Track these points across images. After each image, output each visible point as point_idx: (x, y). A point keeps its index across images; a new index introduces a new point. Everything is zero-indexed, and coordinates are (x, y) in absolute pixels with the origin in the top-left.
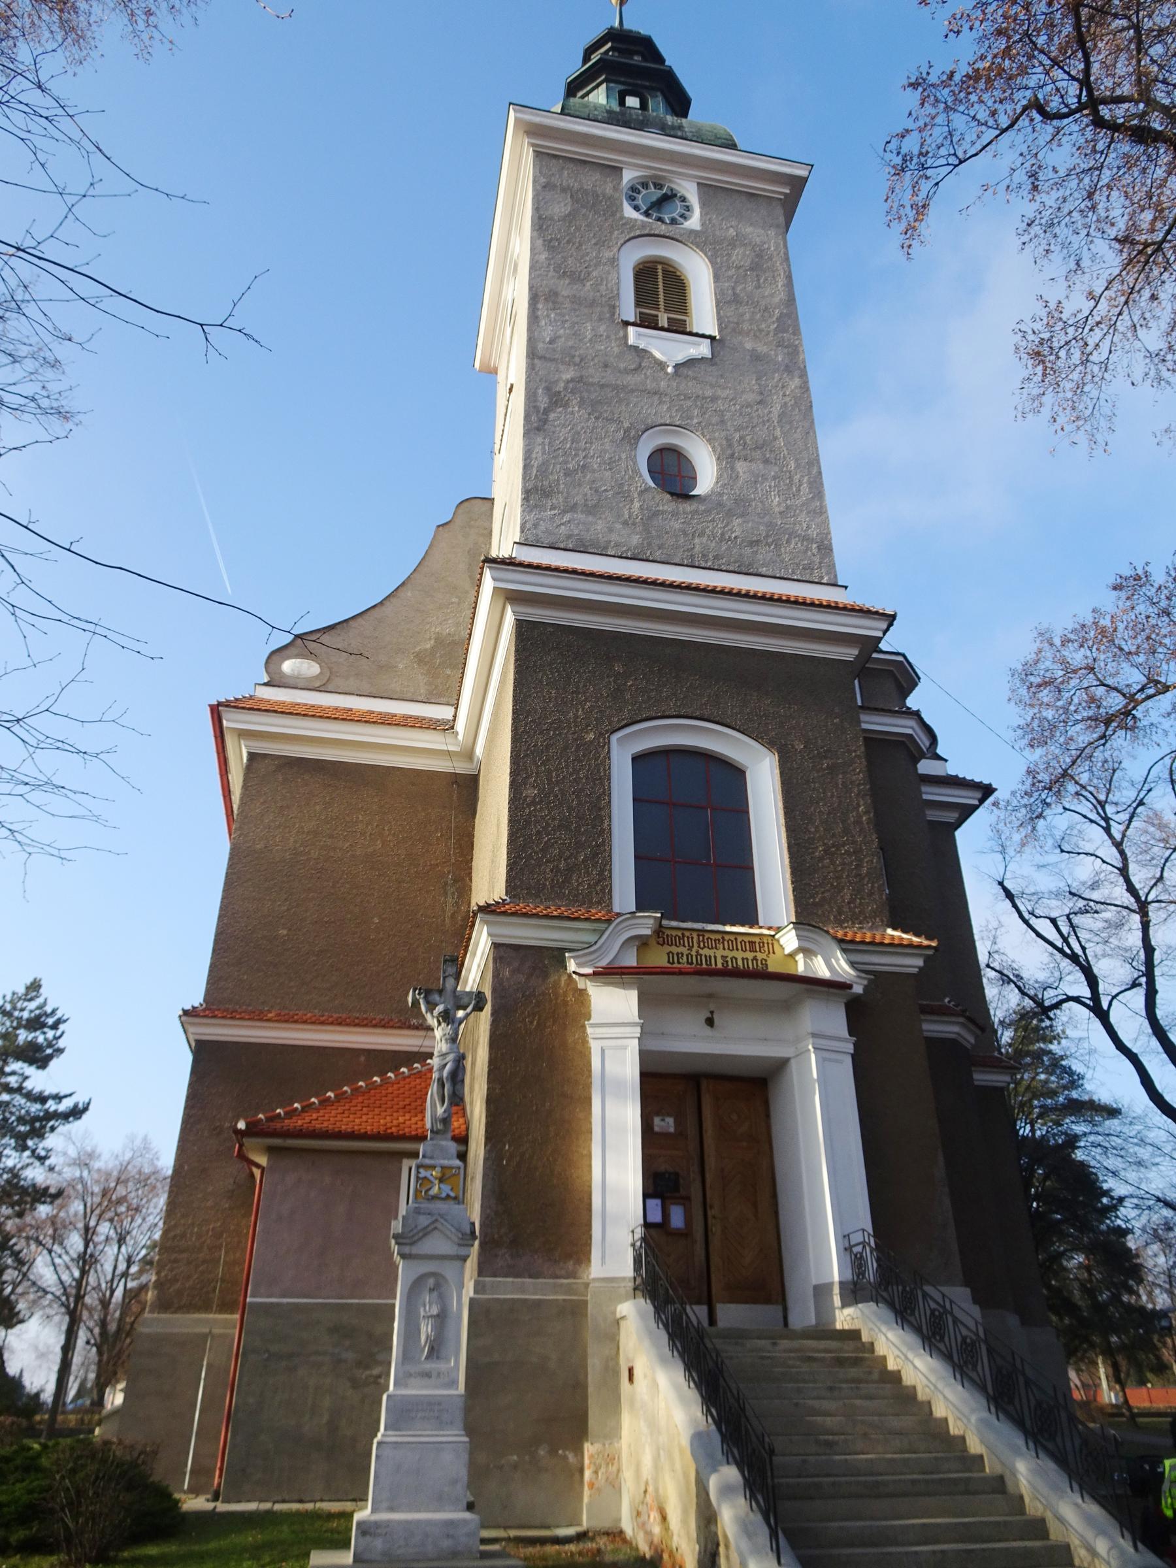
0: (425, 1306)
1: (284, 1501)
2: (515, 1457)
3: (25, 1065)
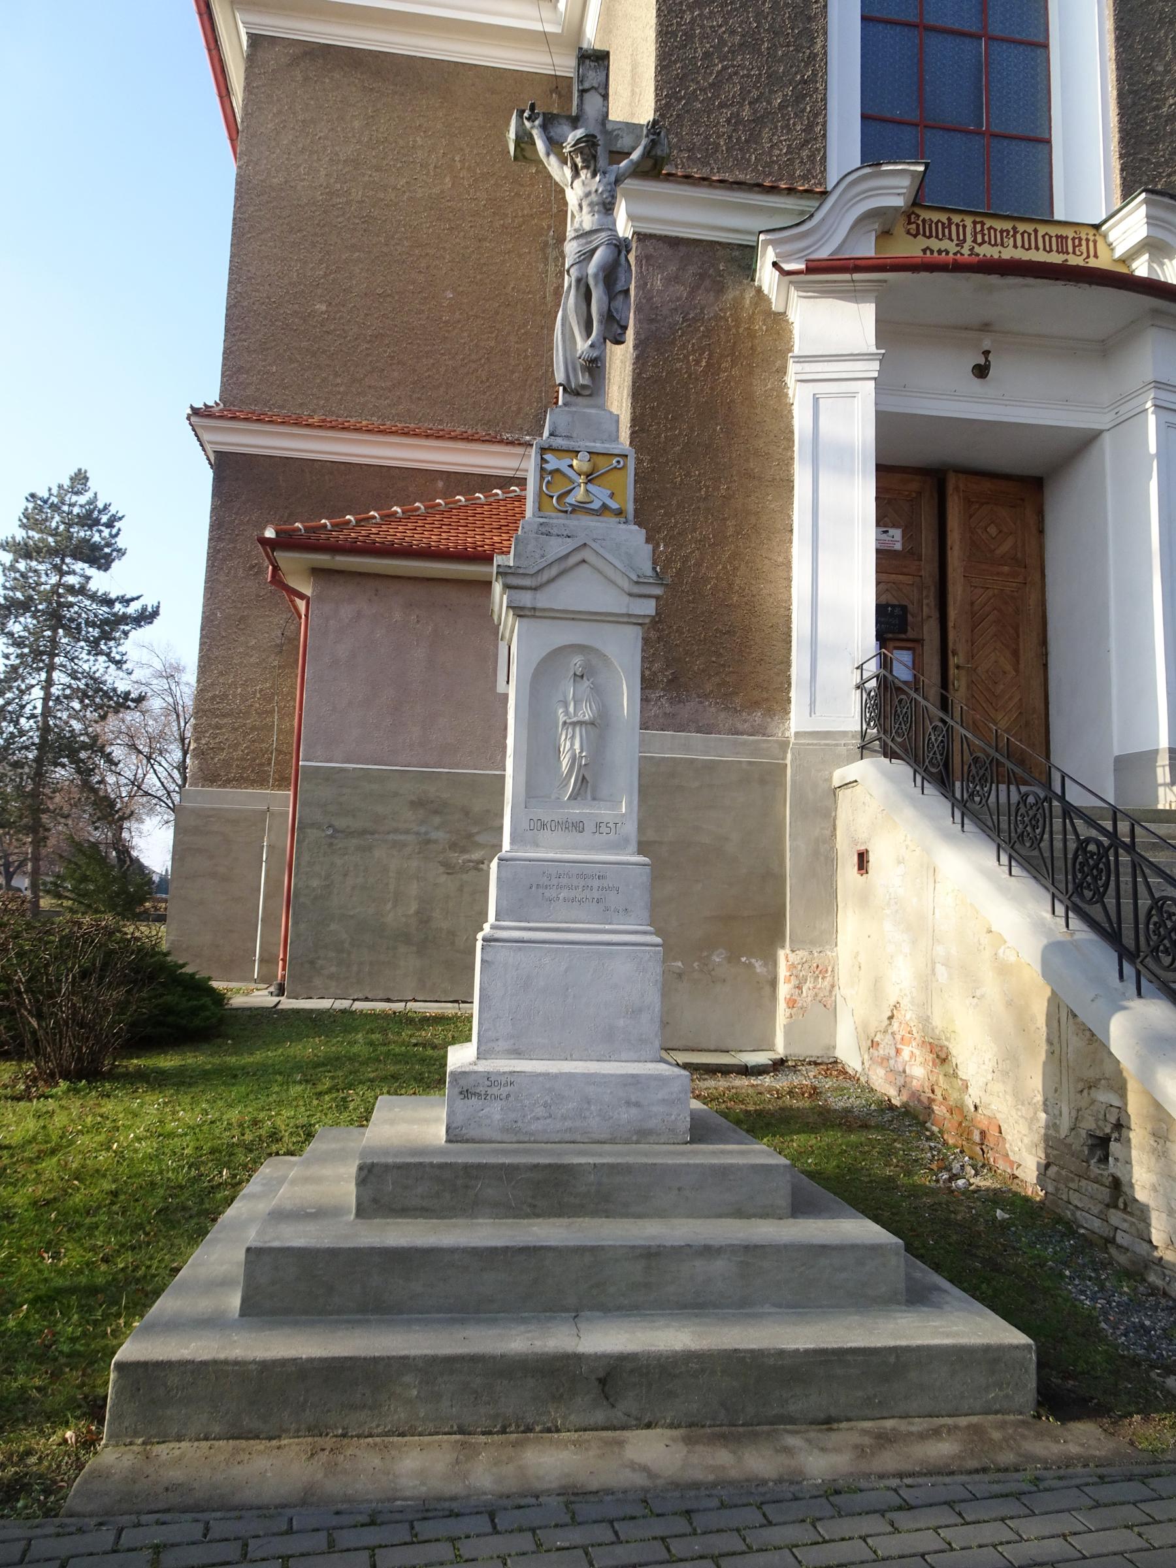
0: (566, 706)
1: (367, 999)
2: (680, 964)
3: (86, 565)
